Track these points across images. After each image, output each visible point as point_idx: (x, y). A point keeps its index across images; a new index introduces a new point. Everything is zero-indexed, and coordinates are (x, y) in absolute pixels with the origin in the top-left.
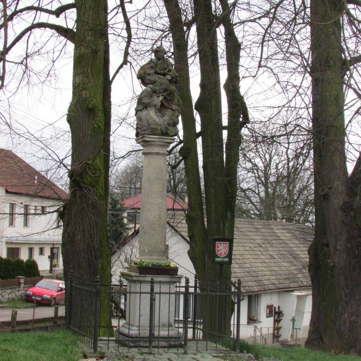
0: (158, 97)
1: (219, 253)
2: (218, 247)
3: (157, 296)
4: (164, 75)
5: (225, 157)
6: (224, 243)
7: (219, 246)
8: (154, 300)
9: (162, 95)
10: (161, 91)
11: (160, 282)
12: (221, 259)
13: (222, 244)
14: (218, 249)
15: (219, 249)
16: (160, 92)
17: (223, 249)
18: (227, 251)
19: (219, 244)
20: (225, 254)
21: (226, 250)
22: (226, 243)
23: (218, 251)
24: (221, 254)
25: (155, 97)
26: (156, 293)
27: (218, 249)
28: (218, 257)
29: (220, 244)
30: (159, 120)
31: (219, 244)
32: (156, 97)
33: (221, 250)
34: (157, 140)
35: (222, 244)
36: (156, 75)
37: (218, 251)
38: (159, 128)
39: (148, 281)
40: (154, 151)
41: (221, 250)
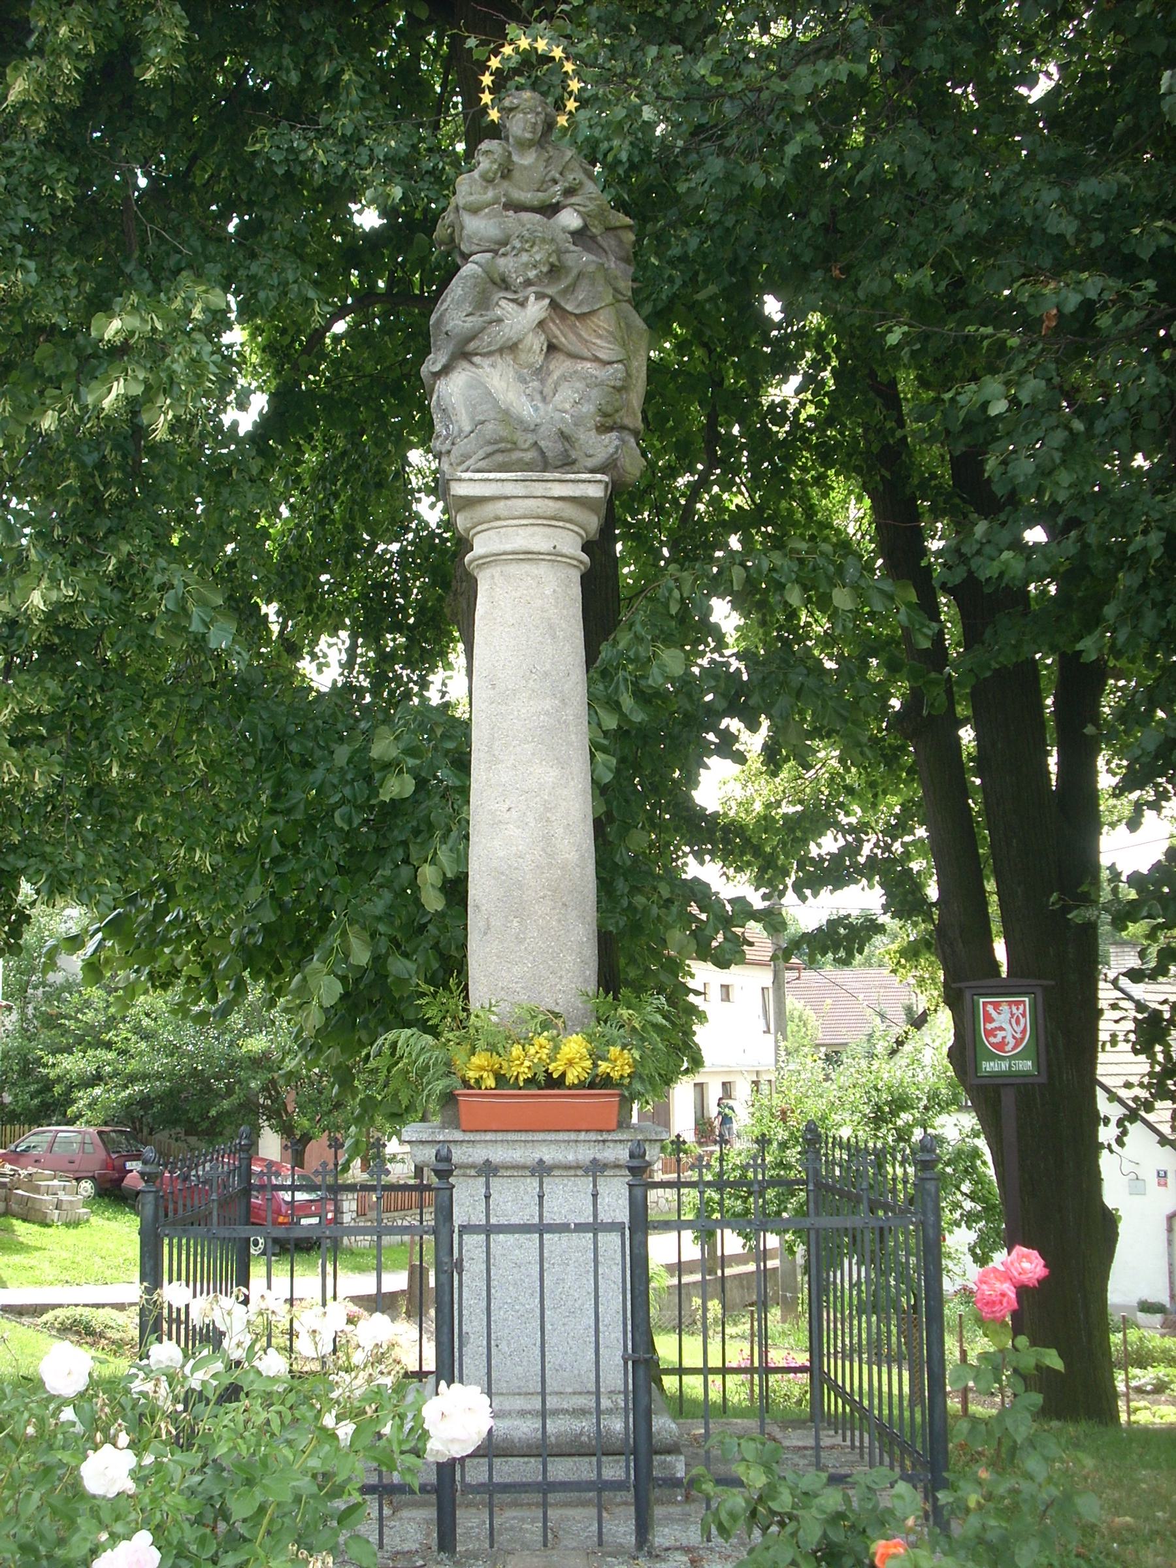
0: (522, 304)
1: (992, 1040)
2: (988, 1018)
3: (473, 1244)
4: (550, 210)
5: (1053, 768)
6: (1010, 1003)
7: (994, 1014)
8: (459, 1266)
9: (540, 296)
10: (532, 274)
11: (488, 1170)
12: (1004, 1066)
13: (1005, 1008)
14: (989, 1026)
15: (993, 1025)
16: (528, 283)
17: (1006, 1026)
18: (1024, 1032)
19: (990, 1008)
20: (1018, 1042)
21: (1019, 1029)
22: (1017, 1003)
23: (990, 1033)
24: (1001, 1046)
25: (503, 303)
26: (465, 1229)
27: (989, 1026)
28: (993, 1057)
29: (996, 1006)
30: (536, 409)
31: (990, 1008)
32: (510, 307)
33: (1001, 1029)
34: (519, 489)
35: (1005, 1008)
36: (511, 213)
37: (990, 1033)
38: (528, 439)
39: (617, 1166)
40: (508, 547)
41: (1001, 1029)
